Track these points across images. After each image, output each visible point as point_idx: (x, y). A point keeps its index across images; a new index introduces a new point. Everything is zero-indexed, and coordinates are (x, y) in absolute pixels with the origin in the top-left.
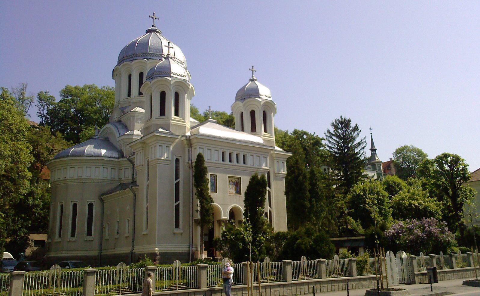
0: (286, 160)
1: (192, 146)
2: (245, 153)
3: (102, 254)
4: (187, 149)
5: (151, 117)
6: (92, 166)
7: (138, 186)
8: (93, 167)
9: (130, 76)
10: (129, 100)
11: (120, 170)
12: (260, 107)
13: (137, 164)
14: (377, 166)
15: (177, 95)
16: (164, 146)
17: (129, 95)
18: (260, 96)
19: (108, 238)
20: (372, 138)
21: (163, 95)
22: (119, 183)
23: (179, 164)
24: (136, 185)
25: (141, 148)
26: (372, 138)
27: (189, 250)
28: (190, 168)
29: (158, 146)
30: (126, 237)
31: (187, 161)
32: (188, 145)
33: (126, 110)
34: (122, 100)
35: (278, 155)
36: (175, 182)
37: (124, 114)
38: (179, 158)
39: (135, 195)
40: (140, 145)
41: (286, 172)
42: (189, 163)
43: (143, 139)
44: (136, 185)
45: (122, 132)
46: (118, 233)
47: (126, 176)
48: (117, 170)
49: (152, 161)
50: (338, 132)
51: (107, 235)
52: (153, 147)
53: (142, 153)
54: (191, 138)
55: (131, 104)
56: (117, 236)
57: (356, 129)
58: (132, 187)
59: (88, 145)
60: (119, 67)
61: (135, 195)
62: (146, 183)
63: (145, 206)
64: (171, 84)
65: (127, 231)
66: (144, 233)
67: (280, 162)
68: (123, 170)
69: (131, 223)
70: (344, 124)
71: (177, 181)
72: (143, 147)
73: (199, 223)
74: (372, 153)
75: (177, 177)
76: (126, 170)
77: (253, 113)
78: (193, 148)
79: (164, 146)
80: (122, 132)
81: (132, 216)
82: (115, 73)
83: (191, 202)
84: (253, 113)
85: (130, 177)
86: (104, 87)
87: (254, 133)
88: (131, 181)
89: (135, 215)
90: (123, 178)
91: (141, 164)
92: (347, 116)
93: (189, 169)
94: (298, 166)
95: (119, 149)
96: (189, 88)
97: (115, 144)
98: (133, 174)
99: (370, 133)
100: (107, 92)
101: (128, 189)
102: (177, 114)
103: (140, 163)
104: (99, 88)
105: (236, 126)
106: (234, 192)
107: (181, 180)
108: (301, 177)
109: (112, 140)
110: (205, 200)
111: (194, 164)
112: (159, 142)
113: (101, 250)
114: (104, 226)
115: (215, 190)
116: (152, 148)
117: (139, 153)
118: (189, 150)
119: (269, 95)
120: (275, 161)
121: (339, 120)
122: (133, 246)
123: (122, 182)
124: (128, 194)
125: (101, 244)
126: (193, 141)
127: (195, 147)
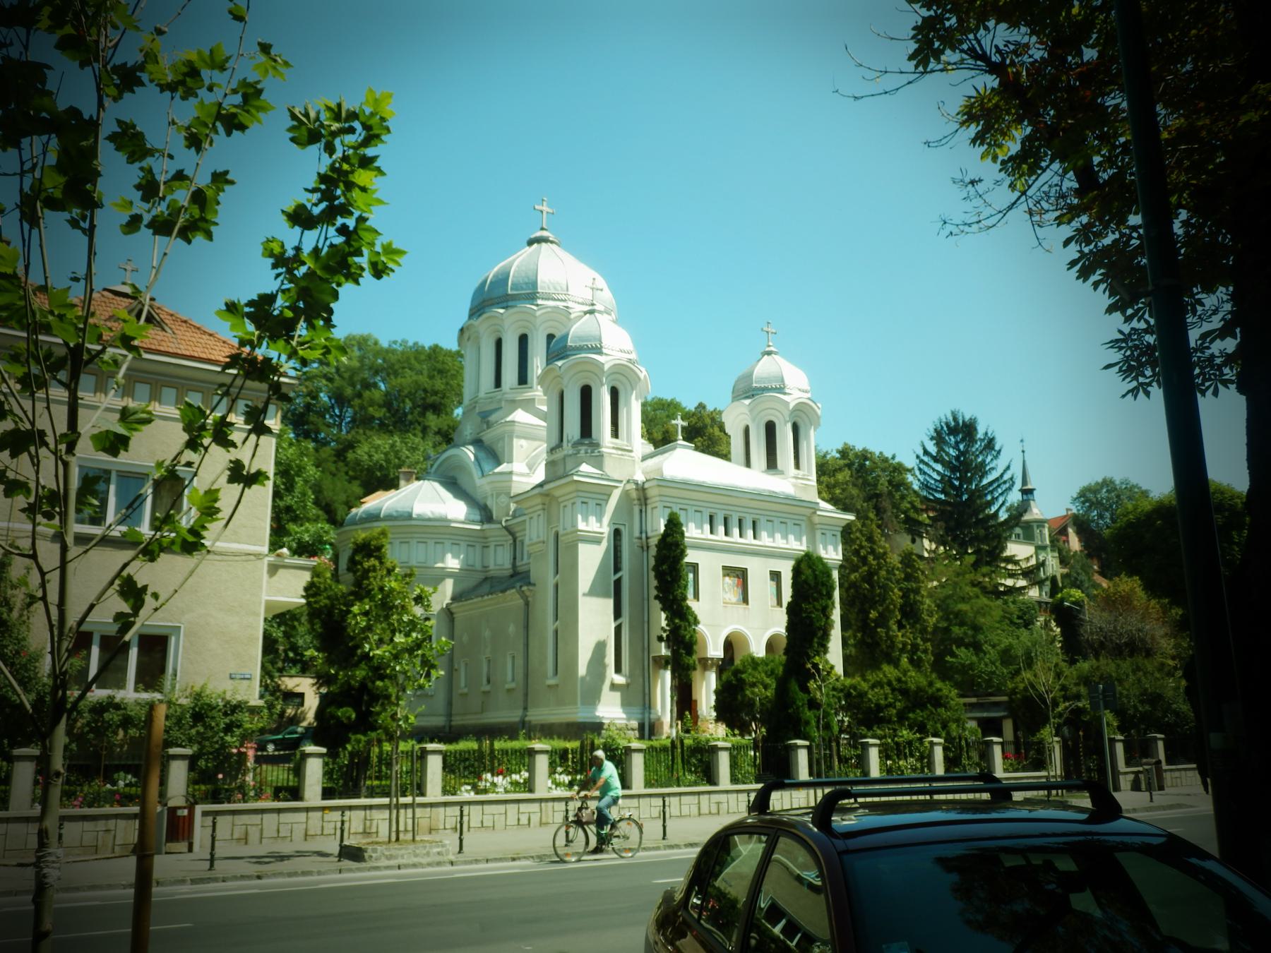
0: (841, 529)
1: (649, 501)
2: (757, 517)
3: (453, 723)
4: (636, 509)
5: (562, 440)
6: (428, 541)
7: (534, 585)
8: (431, 543)
9: (499, 344)
10: (498, 395)
11: (485, 550)
12: (787, 414)
13: (530, 540)
14: (1035, 528)
15: (615, 393)
16: (592, 503)
17: (498, 383)
18: (787, 391)
19: (466, 690)
20: (1024, 461)
21: (586, 394)
22: (482, 576)
23: (620, 540)
24: (529, 584)
25: (540, 507)
26: (1024, 461)
27: (643, 719)
28: (642, 547)
29: (578, 503)
30: (509, 691)
31: (637, 534)
32: (639, 499)
33: (492, 418)
34: (482, 394)
35: (828, 523)
36: (614, 578)
37: (488, 427)
38: (622, 528)
39: (527, 604)
40: (539, 500)
41: (840, 557)
42: (641, 538)
43: (547, 487)
44: (529, 584)
45: (486, 467)
46: (489, 681)
47: (500, 560)
48: (478, 548)
49: (567, 534)
50: (948, 454)
51: (463, 684)
52: (569, 504)
53: (541, 517)
54: (646, 486)
55: (503, 404)
56: (487, 688)
57: (990, 444)
58: (521, 587)
59: (1189, 762)
60: (475, 322)
61: (527, 604)
62: (551, 581)
63: (551, 628)
64: (603, 372)
65: (509, 674)
66: (551, 682)
67: (829, 534)
68: (492, 548)
69: (520, 662)
70: (963, 430)
71: (618, 576)
72: (544, 504)
73: (667, 663)
74: (1025, 497)
75: (617, 568)
76: (498, 548)
77: (770, 429)
78: (649, 507)
79: (592, 503)
80: (486, 467)
81: (521, 647)
82: (466, 335)
83: (646, 619)
84: (770, 429)
85: (508, 565)
86: (395, 342)
87: (772, 472)
88: (511, 572)
89: (527, 645)
90: (492, 567)
91: (541, 539)
92: (967, 414)
93: (640, 550)
94: (875, 547)
95: (482, 502)
96: (639, 379)
97: (470, 490)
98: (515, 558)
99: (1021, 449)
100: (403, 353)
101: (514, 590)
102: (615, 433)
103: (538, 537)
104: (384, 343)
105: (733, 456)
106: (734, 599)
107: (625, 573)
108: (883, 573)
109: (463, 481)
110: (680, 615)
111: (654, 541)
112: (581, 494)
113: (449, 715)
114: (456, 667)
115: (696, 596)
116: (565, 506)
117: (535, 518)
118: (641, 511)
119: (807, 387)
120: (818, 534)
121: (947, 424)
122: (525, 709)
123: (489, 574)
124: (512, 598)
125: (450, 703)
126: (650, 493)
127: (654, 505)
